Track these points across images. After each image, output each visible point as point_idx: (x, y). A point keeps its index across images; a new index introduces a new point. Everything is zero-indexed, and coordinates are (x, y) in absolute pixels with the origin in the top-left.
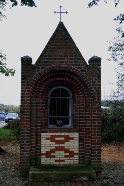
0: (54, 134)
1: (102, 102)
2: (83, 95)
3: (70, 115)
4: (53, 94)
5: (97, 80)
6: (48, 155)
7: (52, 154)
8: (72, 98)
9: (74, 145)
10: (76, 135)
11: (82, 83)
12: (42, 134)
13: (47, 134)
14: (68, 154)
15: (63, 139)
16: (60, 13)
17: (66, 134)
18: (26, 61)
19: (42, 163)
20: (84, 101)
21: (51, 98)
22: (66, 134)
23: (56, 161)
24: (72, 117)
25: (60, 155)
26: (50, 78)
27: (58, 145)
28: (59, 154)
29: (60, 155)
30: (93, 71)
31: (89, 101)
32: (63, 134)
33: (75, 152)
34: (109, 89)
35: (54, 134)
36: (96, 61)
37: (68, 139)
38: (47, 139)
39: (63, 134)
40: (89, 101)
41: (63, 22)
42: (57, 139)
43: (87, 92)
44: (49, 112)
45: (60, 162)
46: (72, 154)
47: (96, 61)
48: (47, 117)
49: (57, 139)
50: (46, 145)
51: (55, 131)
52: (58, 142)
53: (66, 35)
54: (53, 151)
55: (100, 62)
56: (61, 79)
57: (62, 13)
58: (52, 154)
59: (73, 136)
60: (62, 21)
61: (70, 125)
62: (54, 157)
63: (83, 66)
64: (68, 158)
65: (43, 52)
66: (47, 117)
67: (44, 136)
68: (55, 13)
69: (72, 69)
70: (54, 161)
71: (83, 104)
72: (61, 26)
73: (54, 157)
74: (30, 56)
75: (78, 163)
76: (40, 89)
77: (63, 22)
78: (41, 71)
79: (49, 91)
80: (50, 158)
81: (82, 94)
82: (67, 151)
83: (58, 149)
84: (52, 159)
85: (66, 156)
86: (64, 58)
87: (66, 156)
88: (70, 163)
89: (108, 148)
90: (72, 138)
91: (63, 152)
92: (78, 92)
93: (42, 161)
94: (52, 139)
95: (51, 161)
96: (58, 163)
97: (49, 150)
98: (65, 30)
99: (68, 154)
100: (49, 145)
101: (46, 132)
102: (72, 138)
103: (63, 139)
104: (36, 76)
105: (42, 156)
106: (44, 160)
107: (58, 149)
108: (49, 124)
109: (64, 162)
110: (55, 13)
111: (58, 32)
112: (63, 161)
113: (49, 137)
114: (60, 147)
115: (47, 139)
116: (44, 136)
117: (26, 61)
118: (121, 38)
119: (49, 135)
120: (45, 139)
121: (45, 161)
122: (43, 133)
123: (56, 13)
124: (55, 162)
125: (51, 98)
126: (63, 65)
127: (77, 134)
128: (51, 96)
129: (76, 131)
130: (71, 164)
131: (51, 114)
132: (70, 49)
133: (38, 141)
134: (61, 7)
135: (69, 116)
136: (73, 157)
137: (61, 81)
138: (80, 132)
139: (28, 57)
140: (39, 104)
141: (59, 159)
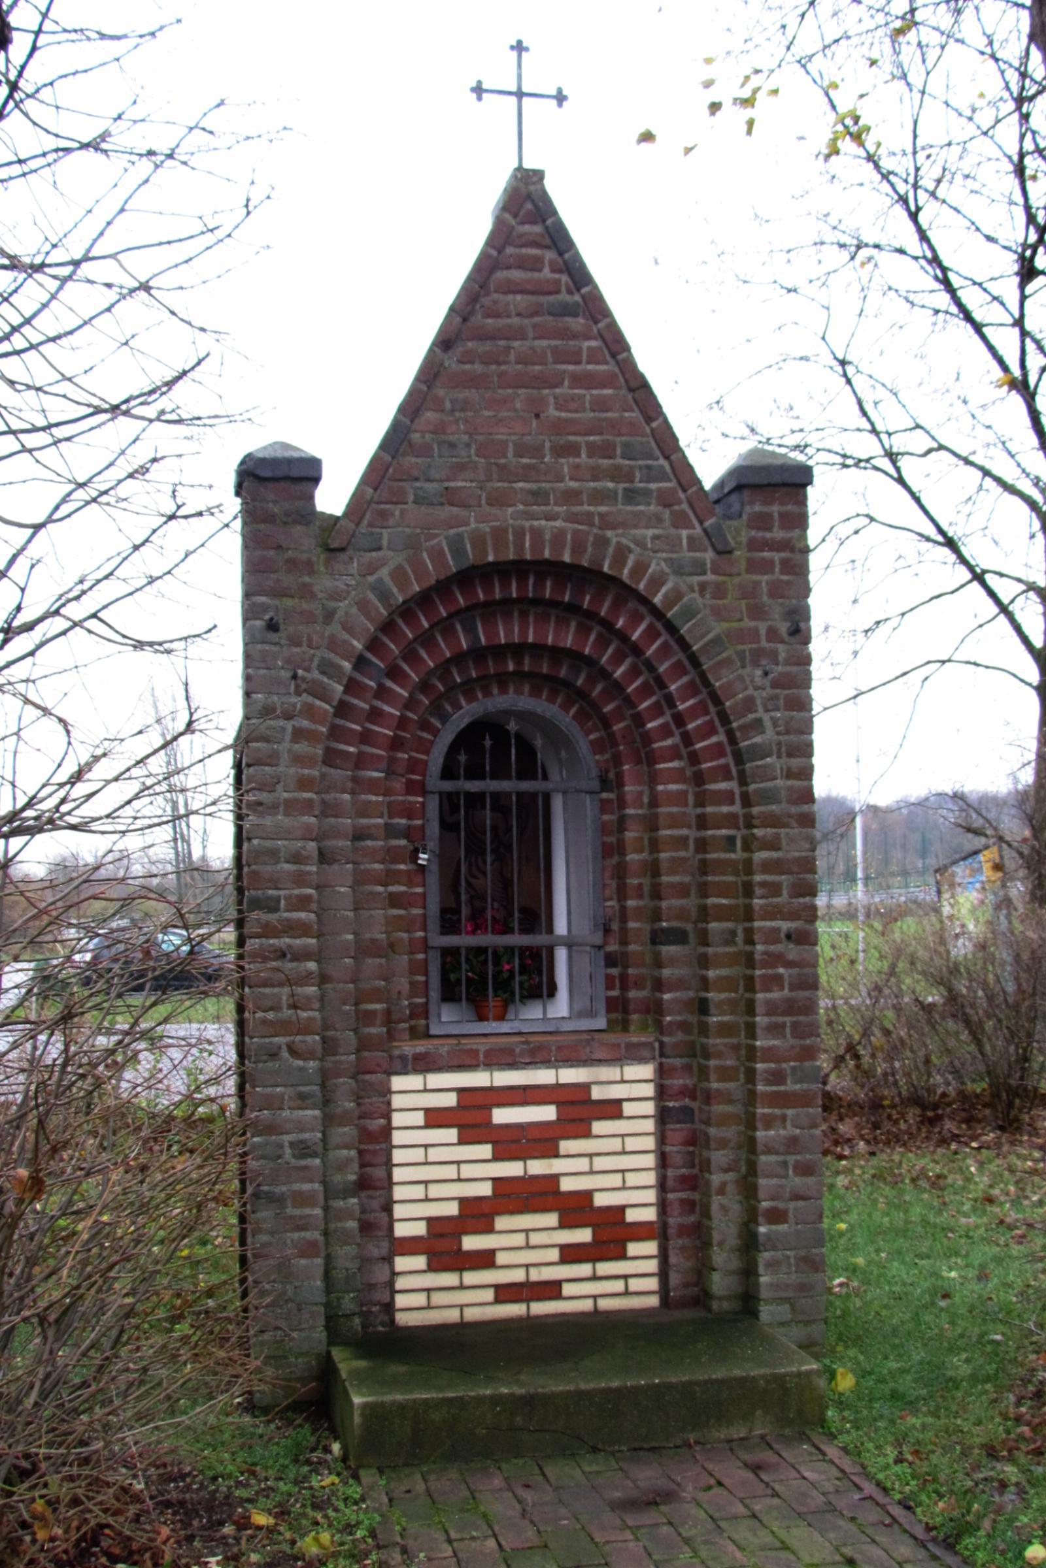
0: (478, 1079)
1: (825, 820)
2: (680, 758)
3: (561, 926)
4: (463, 758)
5: (782, 642)
6: (444, 1247)
7: (471, 1243)
8: (595, 785)
9: (619, 1165)
10: (633, 1084)
11: (679, 663)
12: (398, 1082)
13: (436, 1080)
14: (583, 1235)
15: (547, 1113)
16: (525, 100)
17: (570, 1075)
18: (274, 485)
19: (402, 1319)
20: (692, 811)
21: (448, 786)
22: (570, 1075)
23: (504, 1293)
24: (598, 939)
25: (526, 1245)
26: (445, 627)
27: (512, 1169)
28: (519, 1240)
29: (526, 1245)
30: (755, 566)
31: (725, 809)
32: (544, 1076)
33: (632, 1216)
34: (905, 710)
35: (478, 1079)
36: (774, 489)
37: (580, 1112)
38: (435, 1118)
39: (544, 1076)
40: (725, 809)
41: (539, 175)
42: (502, 1116)
43: (714, 739)
44: (434, 905)
45: (528, 1300)
46: (611, 1234)
47: (774, 489)
48: (425, 946)
49: (502, 1116)
50: (432, 1172)
51: (488, 1053)
52: (511, 1143)
53: (564, 278)
54: (477, 1215)
55: (802, 502)
56: (524, 631)
57: (525, 89)
58: (471, 1243)
59: (616, 1092)
60: (527, 165)
61: (560, 1006)
62: (486, 1259)
63: (684, 533)
64: (585, 1269)
65: (402, 409)
66: (425, 946)
67: (413, 1094)
68: (560, 91)
69: (611, 550)
70: (489, 1295)
71: (684, 832)
72: (529, 206)
73: (486, 1259)
74: (310, 447)
75: (654, 1301)
76: (375, 715)
77: (539, 175)
78: (392, 565)
79: (435, 732)
80: (461, 1269)
81: (674, 754)
82: (575, 1209)
83: (516, 1196)
84: (470, 1277)
85: (570, 1254)
86: (559, 456)
87: (570, 1254)
88: (604, 1304)
89: (884, 1156)
90: (612, 1109)
91: (552, 1219)
92: (647, 738)
93: (401, 1301)
94: (469, 1118)
95: (467, 1299)
96: (515, 1310)
97: (452, 1209)
98: (558, 239)
99: (583, 1235)
100: (450, 1172)
101: (423, 1064)
102: (612, 1109)
103: (547, 1113)
104: (353, 598)
105: (402, 1263)
106: (422, 1295)
107: (516, 1196)
108: (434, 994)
109: (558, 1296)
110: (560, 91)
111: (509, 250)
112: (552, 1290)
113: (450, 1100)
114: (536, 1177)
115: (435, 1118)
116: (413, 1094)
117: (274, 485)
118: (210, 476)
119: (444, 1087)
120: (421, 1122)
121: (420, 1299)
122: (404, 1072)
123: (554, 93)
124: (498, 1300)
125: (448, 786)
126: (549, 517)
127: (646, 1071)
128: (448, 773)
129: (632, 1055)
130: (608, 1313)
131: (449, 924)
132: (595, 392)
133: (376, 1142)
134: (519, 47)
135: (550, 930)
136: (622, 1256)
137: (518, 650)
138: (662, 1055)
139: (296, 455)
140: (369, 843)
141: (518, 1276)
